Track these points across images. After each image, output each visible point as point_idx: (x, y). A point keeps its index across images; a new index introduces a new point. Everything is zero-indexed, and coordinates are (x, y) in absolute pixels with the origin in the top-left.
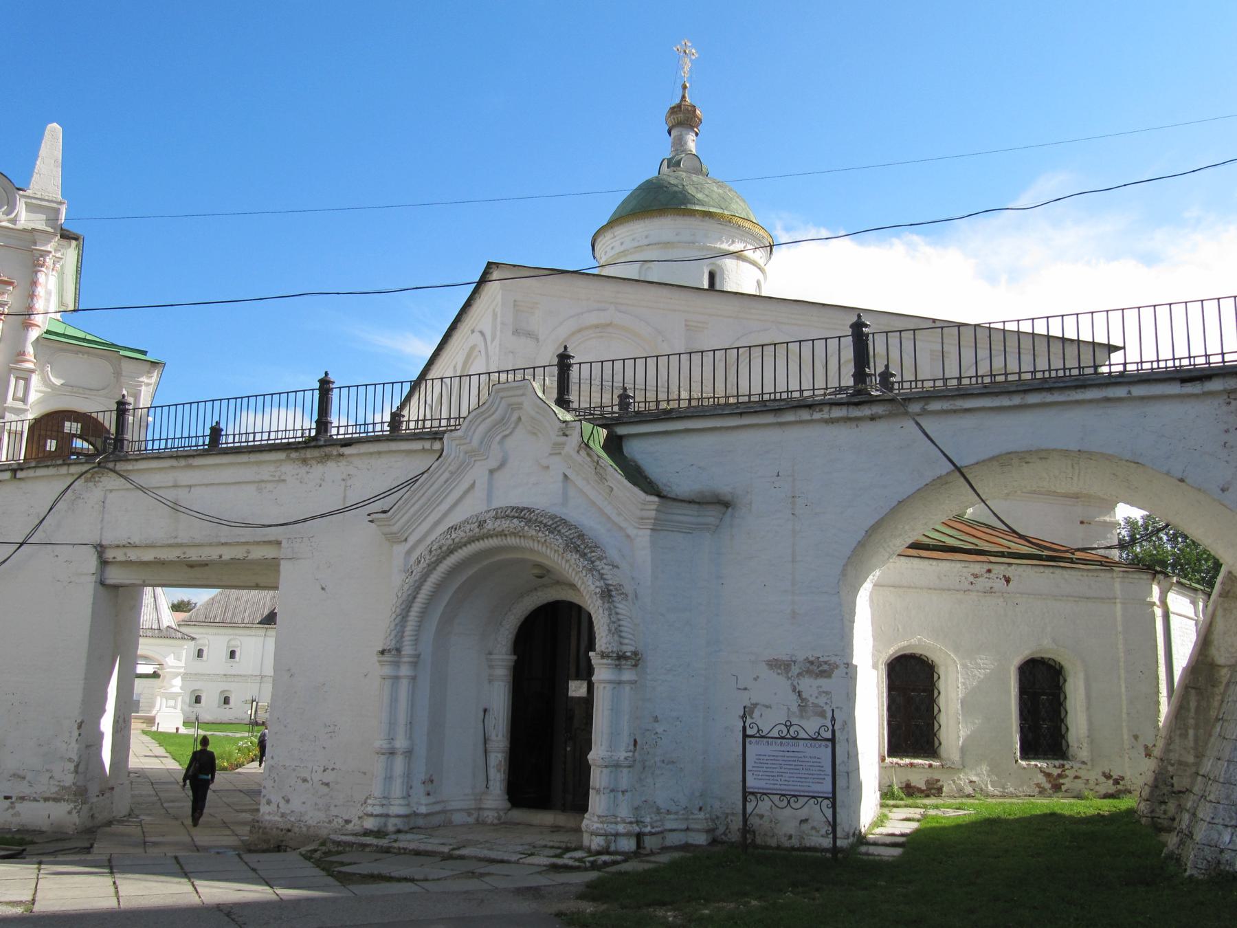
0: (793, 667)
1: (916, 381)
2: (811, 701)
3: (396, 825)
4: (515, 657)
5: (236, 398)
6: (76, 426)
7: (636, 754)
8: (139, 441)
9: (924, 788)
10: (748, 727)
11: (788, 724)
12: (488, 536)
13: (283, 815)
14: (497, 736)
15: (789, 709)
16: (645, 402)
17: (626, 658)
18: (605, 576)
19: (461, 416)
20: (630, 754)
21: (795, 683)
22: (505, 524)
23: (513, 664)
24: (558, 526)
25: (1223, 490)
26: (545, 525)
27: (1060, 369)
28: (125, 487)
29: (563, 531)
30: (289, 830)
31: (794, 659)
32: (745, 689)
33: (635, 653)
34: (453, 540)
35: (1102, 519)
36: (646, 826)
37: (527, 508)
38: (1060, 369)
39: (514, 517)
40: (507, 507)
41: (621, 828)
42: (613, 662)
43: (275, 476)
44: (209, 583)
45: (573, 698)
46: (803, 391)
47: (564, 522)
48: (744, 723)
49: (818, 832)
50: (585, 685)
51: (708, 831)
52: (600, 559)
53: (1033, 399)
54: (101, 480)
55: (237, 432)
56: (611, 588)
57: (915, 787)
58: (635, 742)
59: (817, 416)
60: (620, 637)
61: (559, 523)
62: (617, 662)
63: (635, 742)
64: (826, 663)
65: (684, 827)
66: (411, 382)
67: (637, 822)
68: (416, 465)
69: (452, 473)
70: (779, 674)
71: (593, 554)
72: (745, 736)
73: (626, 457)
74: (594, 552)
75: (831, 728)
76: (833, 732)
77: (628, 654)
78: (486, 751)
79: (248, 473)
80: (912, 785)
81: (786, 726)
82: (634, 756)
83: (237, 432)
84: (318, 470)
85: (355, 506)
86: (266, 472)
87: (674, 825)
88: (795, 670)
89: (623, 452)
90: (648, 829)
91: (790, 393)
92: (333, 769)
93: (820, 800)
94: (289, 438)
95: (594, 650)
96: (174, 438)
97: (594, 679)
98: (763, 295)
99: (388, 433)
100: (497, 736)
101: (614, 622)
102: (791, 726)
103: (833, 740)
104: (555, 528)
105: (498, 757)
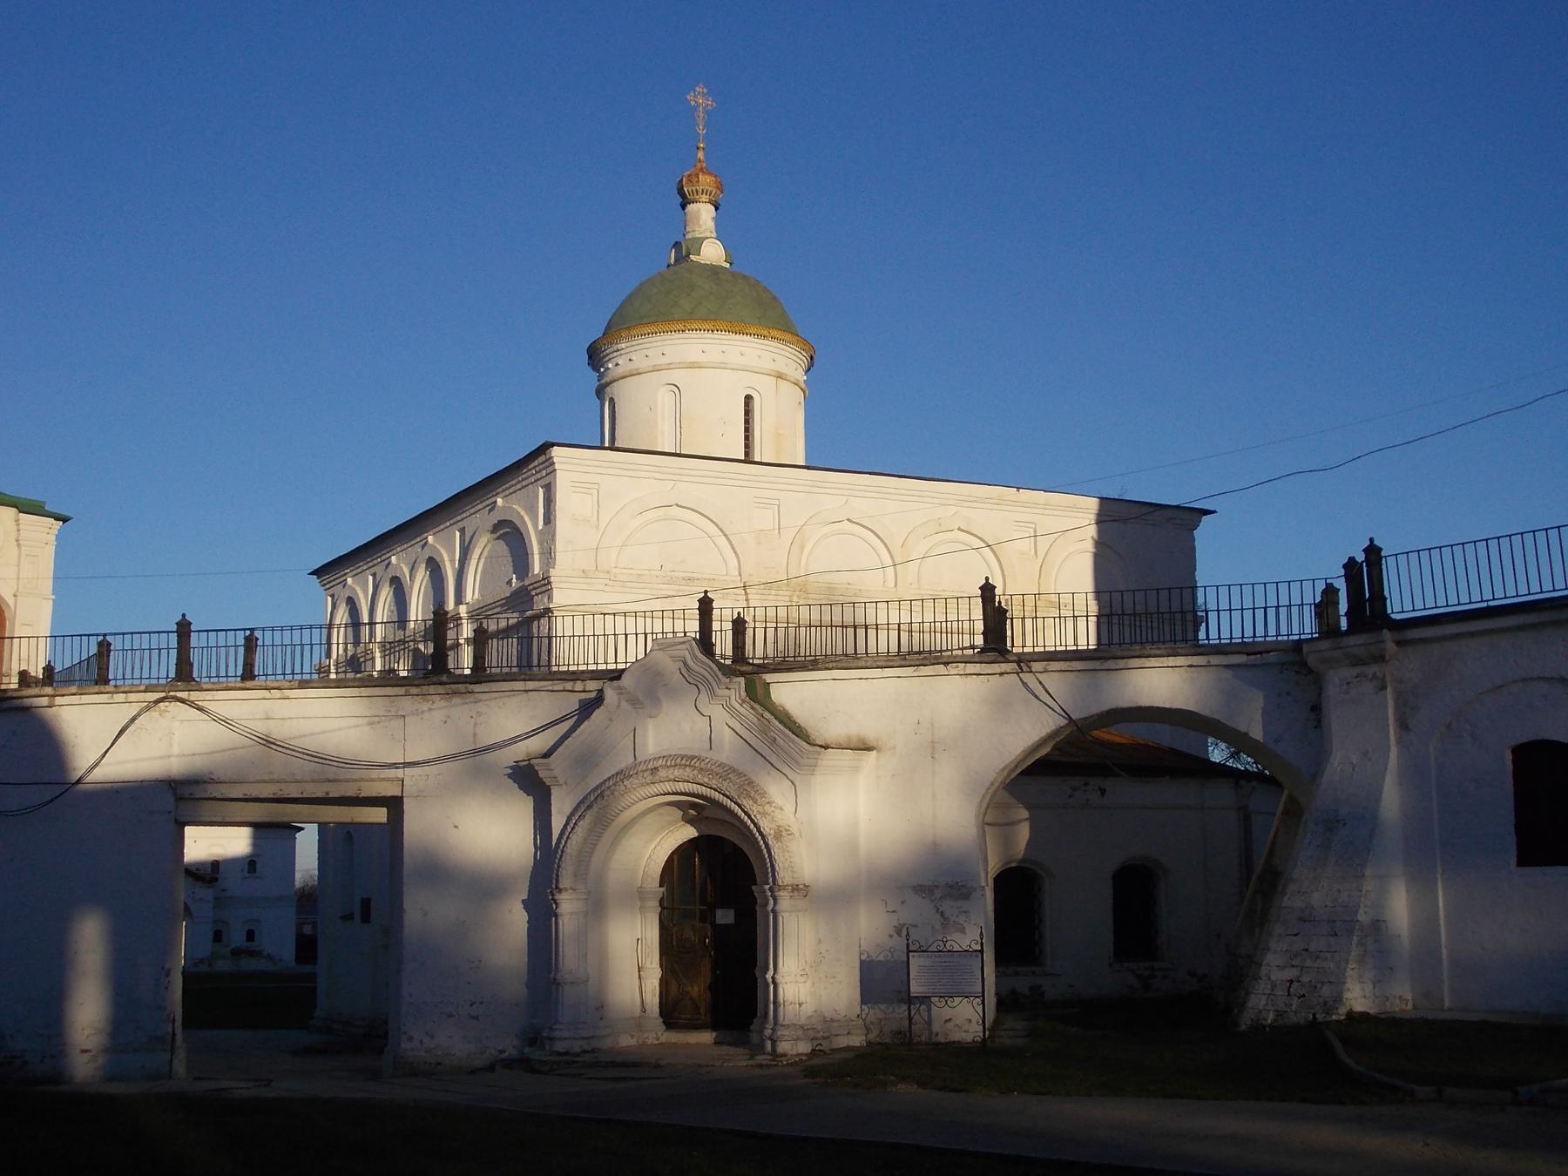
3: (581, 1046)
10: (911, 944)
11: (945, 939)
14: (651, 963)
15: (933, 927)
21: (938, 905)
27: (172, 632)
28: (202, 718)
30: (439, 1064)
31: (936, 884)
35: (697, 855)
36: (819, 1032)
38: (172, 632)
43: (390, 711)
49: (961, 1028)
54: (168, 709)
70: (923, 898)
81: (890, 951)
88: (938, 894)
92: (481, 1003)
93: (972, 999)
94: (963, 649)
98: (12, 511)
99: (1317, 635)
100: (651, 963)
102: (894, 951)
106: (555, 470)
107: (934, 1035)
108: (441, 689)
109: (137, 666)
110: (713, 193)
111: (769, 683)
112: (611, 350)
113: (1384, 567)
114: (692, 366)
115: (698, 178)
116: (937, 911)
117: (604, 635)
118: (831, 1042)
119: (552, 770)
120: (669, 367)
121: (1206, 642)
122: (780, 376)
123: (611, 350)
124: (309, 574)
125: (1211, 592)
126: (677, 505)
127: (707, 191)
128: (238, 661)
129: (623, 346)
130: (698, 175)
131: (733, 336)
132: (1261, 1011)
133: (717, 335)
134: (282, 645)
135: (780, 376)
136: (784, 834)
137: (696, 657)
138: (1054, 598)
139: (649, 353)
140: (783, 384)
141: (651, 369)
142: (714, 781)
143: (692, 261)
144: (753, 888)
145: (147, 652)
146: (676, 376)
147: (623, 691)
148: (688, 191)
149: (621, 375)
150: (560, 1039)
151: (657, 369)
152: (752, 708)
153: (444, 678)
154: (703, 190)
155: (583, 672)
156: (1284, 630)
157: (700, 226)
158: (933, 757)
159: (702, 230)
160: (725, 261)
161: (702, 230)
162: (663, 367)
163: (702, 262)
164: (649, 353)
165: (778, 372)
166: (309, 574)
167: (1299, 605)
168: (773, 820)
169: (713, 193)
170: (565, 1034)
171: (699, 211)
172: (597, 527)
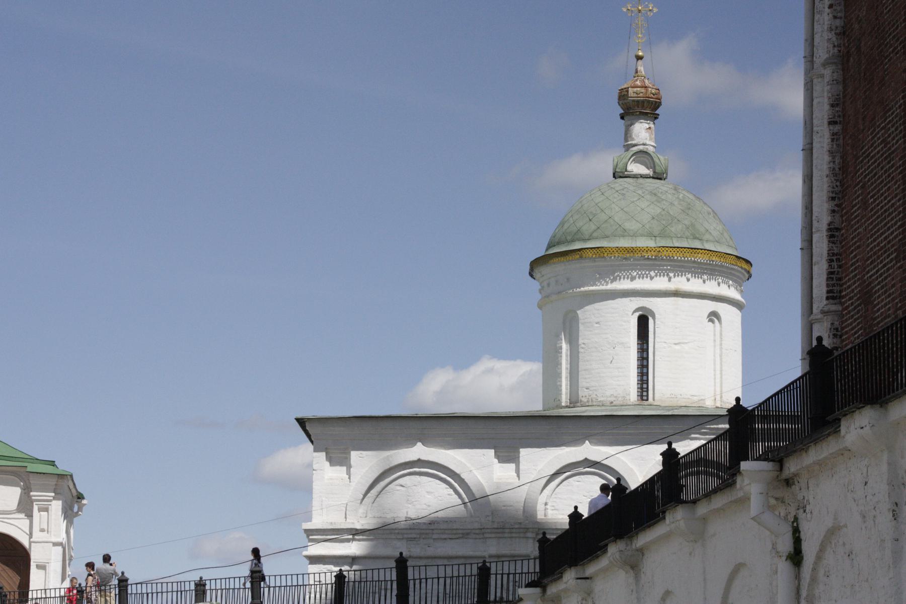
1: (379, 581)
5: (226, 579)
6: (38, 595)
8: (190, 590)
16: (445, 577)
19: (530, 572)
27: (393, 568)
38: (393, 568)
44: (259, 592)
46: (421, 579)
55: (183, 589)
66: (65, 588)
69: (516, 582)
83: (179, 590)
91: (380, 582)
96: (522, 573)
107: (634, 591)
109: (499, 582)
117: (385, 581)
125: (272, 578)
128: (504, 579)
134: (325, 584)
138: (114, 586)
145: (219, 591)
167: (514, 574)
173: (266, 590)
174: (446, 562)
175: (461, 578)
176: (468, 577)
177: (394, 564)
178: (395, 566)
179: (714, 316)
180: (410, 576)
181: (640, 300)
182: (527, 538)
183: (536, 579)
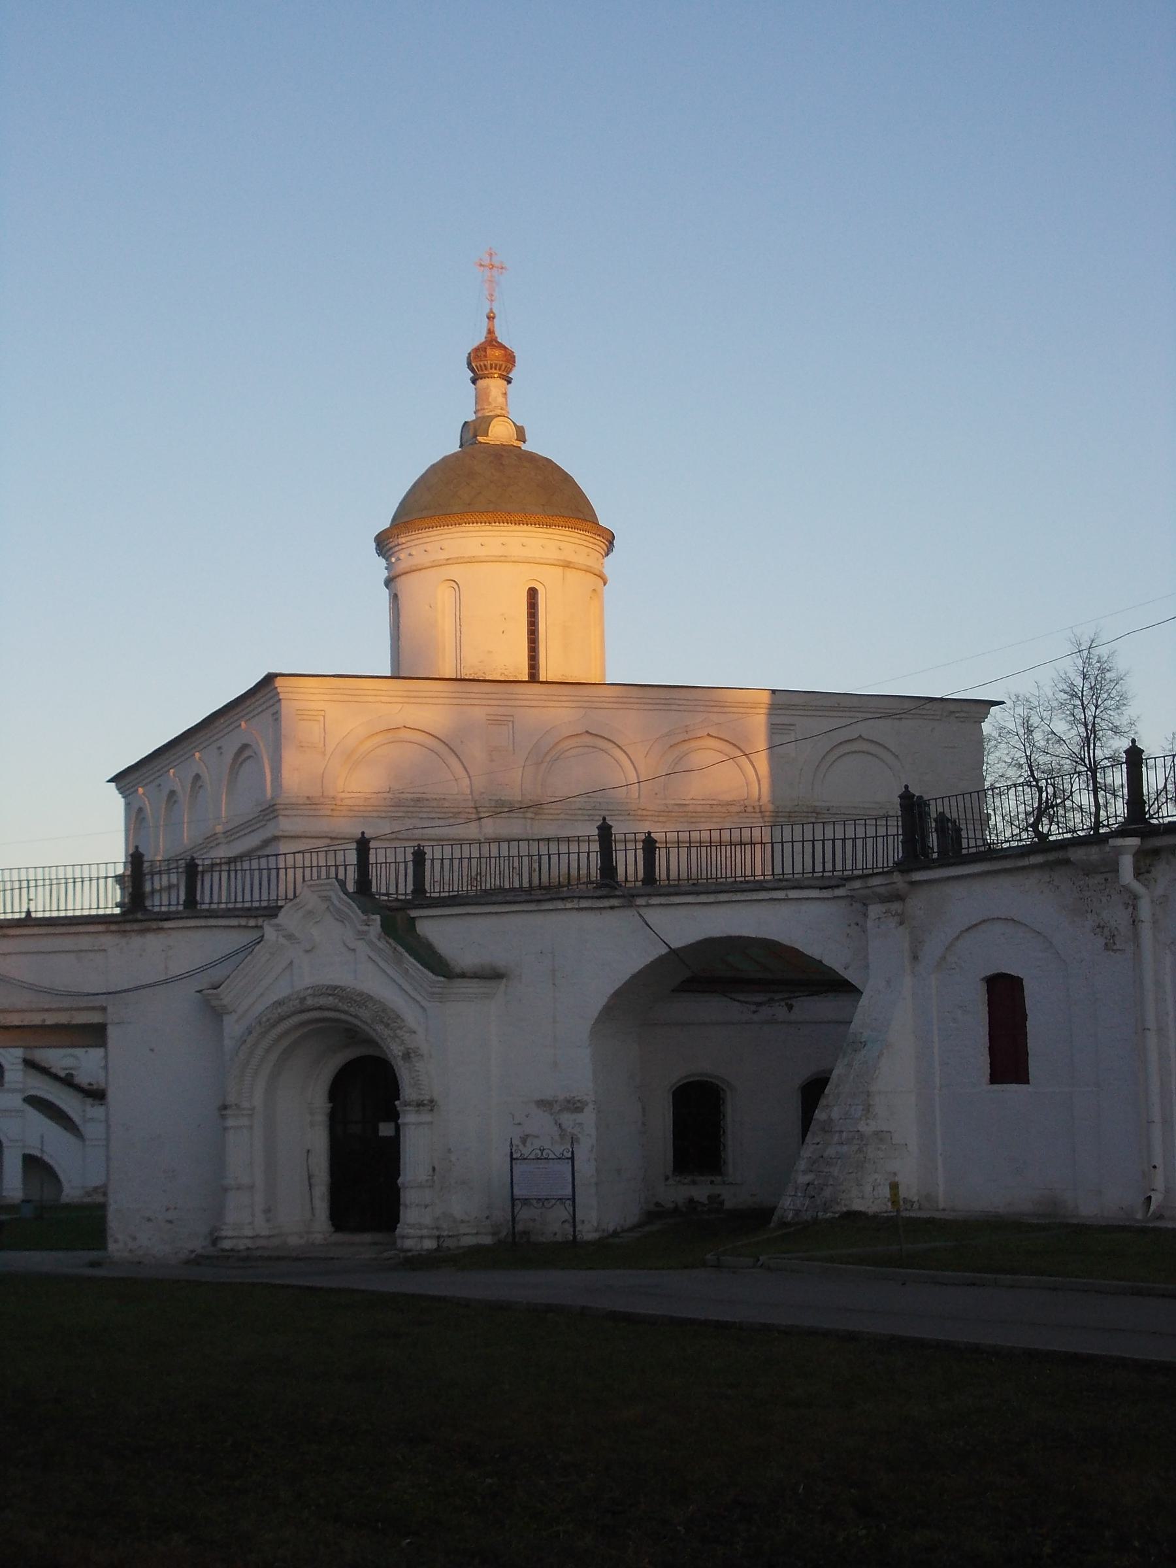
0: (555, 1106)
2: (569, 1131)
4: (331, 1105)
7: (435, 1178)
9: (706, 1202)
11: (542, 1148)
12: (309, 1010)
13: (131, 1251)
17: (424, 1105)
18: (405, 1042)
20: (431, 1178)
22: (322, 1001)
23: (329, 1110)
24: (366, 1002)
25: (845, 968)
26: (355, 1001)
29: (370, 1006)
31: (556, 1099)
32: (520, 1124)
33: (431, 1101)
34: (279, 1014)
37: (339, 987)
39: (330, 995)
40: (323, 985)
41: (425, 1232)
42: (413, 1109)
45: (381, 1137)
47: (370, 998)
48: (511, 1149)
50: (392, 1125)
51: (494, 1234)
52: (401, 1028)
53: (723, 897)
56: (410, 1051)
57: (697, 1202)
58: (434, 1169)
59: (569, 906)
60: (419, 1089)
61: (366, 999)
62: (417, 1109)
63: (434, 1169)
64: (579, 1101)
65: (475, 1231)
67: (437, 1228)
68: (238, 939)
71: (395, 1024)
72: (512, 1159)
73: (419, 935)
74: (395, 1022)
75: (571, 1150)
76: (573, 1152)
77: (425, 1102)
78: (310, 1185)
79: (68, 943)
80: (695, 1200)
82: (432, 1179)
84: (137, 941)
85: (179, 978)
86: (85, 942)
87: (467, 1231)
88: (557, 1108)
89: (416, 931)
90: (445, 1233)
92: (175, 1208)
95: (399, 1099)
97: (400, 1121)
101: (413, 1078)
103: (572, 1158)
104: (364, 1003)
105: (321, 1189)
106: (280, 700)
108: (136, 926)
110: (503, 367)
111: (414, 918)
112: (393, 544)
113: (657, 856)
114: (471, 561)
115: (486, 352)
116: (556, 1123)
118: (459, 1240)
119: (221, 999)
120: (448, 562)
121: (791, 876)
122: (567, 565)
123: (393, 544)
124: (108, 781)
126: (405, 727)
127: (496, 365)
129: (403, 540)
130: (486, 348)
131: (517, 528)
132: (785, 1210)
133: (497, 527)
134: (396, 862)
135: (567, 565)
136: (412, 1055)
137: (340, 897)
139: (428, 547)
140: (571, 574)
141: (430, 565)
142: (352, 1009)
143: (480, 442)
144: (397, 1103)
145: (265, 872)
146: (454, 572)
147: (280, 928)
148: (476, 366)
149: (402, 571)
150: (226, 1238)
151: (435, 565)
152: (387, 942)
153: (139, 916)
154: (491, 365)
155: (257, 909)
156: (839, 867)
157: (490, 404)
158: (554, 984)
159: (491, 407)
160: (517, 440)
161: (491, 407)
162: (441, 563)
163: (491, 442)
164: (428, 547)
165: (565, 561)
166: (108, 781)
168: (403, 1042)
169: (503, 367)
170: (230, 1233)
171: (488, 387)
172: (324, 754)
173: (663, 851)
174: (387, 844)
175: (493, 860)
176: (494, 859)
177: (354, 846)
178: (597, 834)
179: (839, 704)
180: (372, 859)
181: (471, 674)
182: (525, 818)
183: (1093, 826)
